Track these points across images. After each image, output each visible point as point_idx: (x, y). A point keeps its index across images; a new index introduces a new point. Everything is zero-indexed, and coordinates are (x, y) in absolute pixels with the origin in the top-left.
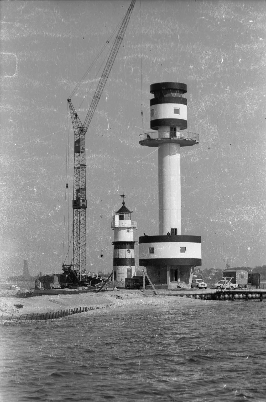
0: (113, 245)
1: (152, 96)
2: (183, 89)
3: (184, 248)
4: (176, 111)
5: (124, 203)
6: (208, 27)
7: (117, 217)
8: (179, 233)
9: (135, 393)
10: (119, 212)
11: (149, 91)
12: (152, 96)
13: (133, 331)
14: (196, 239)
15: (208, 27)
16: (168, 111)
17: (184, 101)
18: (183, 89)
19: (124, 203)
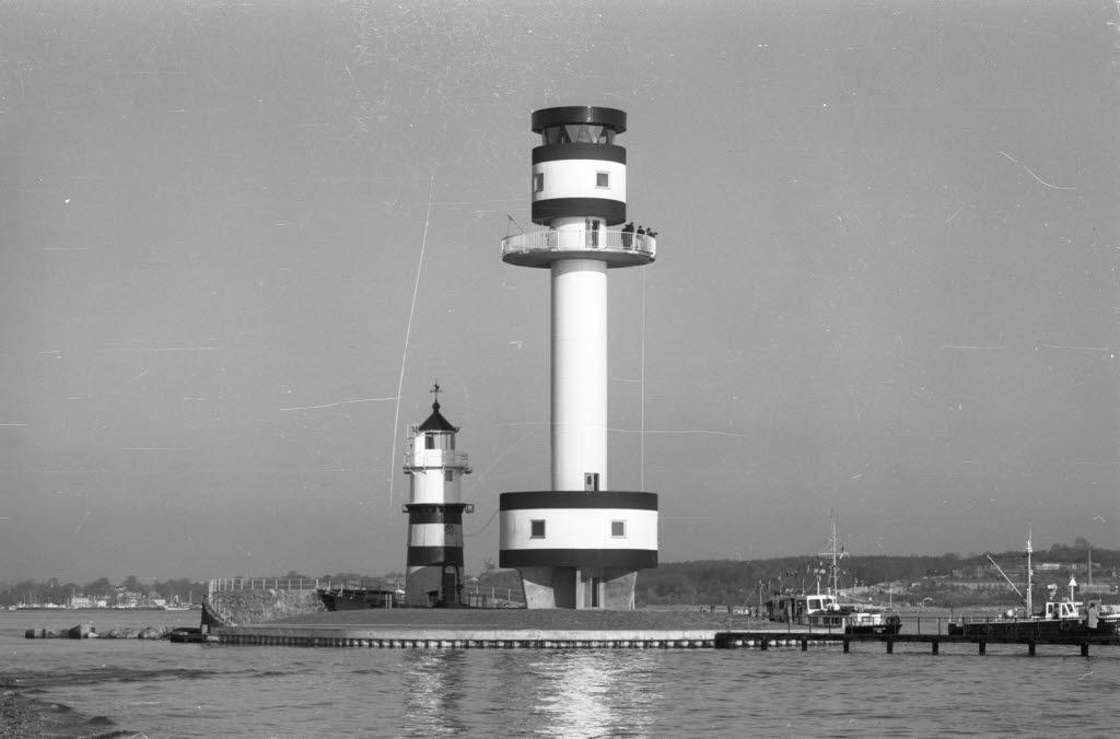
0: (408, 514)
1: (538, 140)
2: (612, 120)
3: (430, 510)
4: (602, 179)
5: (436, 406)
6: (1050, 587)
7: (421, 440)
8: (603, 487)
9: (1003, 578)
10: (422, 428)
11: (530, 128)
12: (538, 140)
13: (964, 580)
14: (645, 501)
15: (1050, 587)
16: (571, 178)
17: (619, 155)
18: (612, 120)
19: (436, 406)
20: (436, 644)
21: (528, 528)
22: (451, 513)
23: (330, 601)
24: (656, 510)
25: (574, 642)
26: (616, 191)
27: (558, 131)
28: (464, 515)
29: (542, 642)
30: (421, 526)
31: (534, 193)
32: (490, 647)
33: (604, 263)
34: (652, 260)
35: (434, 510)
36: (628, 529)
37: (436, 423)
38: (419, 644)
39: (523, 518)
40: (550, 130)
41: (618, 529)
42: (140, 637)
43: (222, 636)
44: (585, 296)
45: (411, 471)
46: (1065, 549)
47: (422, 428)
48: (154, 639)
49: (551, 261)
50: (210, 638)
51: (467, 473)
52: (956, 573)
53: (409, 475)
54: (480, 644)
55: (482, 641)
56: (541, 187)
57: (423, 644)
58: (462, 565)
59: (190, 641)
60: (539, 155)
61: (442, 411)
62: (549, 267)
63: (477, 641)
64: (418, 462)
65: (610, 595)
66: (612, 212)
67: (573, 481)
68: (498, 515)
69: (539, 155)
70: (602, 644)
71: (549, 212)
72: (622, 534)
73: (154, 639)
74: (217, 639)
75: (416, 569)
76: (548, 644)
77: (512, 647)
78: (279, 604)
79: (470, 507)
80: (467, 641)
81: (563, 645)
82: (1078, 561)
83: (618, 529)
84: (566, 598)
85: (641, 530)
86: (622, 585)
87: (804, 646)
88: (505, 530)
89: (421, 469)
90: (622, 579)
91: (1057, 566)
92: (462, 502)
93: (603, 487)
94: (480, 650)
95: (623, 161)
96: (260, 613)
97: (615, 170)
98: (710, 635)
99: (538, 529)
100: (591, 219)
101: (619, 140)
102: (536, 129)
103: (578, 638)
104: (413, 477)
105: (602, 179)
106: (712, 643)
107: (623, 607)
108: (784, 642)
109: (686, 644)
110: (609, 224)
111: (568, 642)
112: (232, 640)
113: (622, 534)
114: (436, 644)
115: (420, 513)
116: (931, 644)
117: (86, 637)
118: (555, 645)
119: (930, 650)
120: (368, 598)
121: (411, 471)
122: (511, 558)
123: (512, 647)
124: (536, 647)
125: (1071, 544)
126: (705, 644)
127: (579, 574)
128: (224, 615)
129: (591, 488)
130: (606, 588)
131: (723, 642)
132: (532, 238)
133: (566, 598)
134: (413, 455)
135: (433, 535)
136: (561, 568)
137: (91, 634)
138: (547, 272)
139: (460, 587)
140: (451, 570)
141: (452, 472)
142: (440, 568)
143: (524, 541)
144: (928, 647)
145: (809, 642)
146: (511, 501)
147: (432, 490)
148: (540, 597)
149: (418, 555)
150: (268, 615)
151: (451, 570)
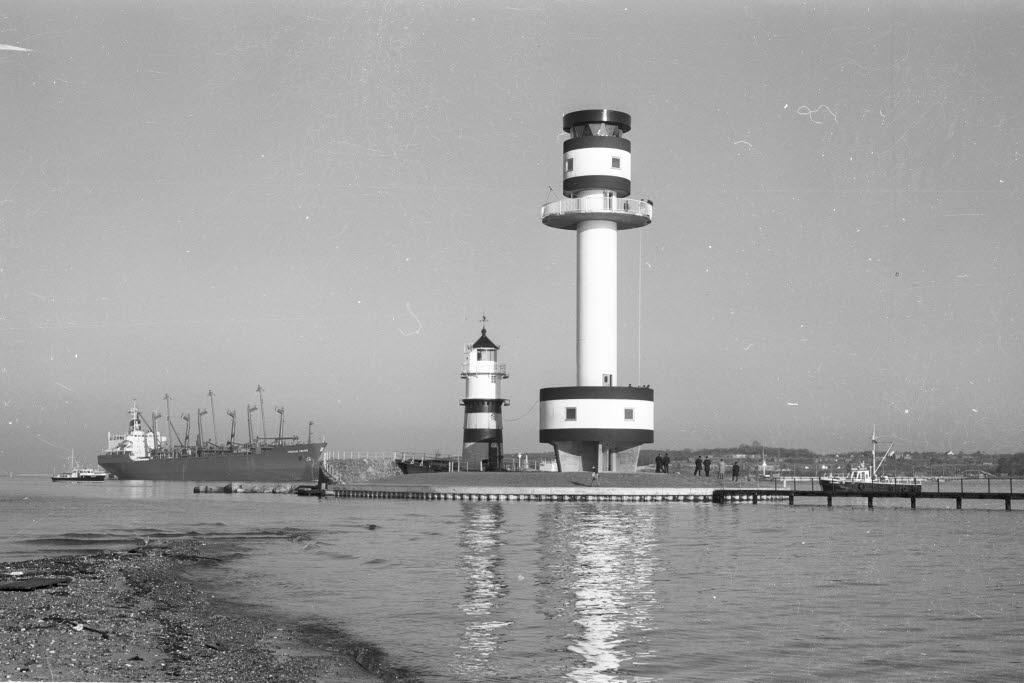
1: (568, 136)
2: (621, 122)
4: (616, 162)
5: (484, 331)
7: (474, 353)
10: (475, 346)
12: (568, 136)
14: (645, 394)
16: (592, 161)
18: (621, 122)
19: (484, 331)
20: (505, 497)
21: (564, 414)
22: (496, 406)
23: (404, 467)
24: (651, 399)
25: (610, 496)
26: (624, 172)
27: (580, 127)
28: (503, 406)
29: (586, 496)
30: (473, 415)
31: (565, 173)
32: (546, 500)
33: (614, 225)
34: (649, 222)
35: (483, 404)
36: (635, 414)
37: (483, 342)
38: (492, 497)
39: (559, 407)
40: (577, 128)
41: (629, 414)
42: (274, 492)
43: (336, 491)
44: (601, 242)
45: (466, 376)
46: (747, 447)
47: (475, 346)
48: (284, 493)
49: (573, 222)
50: (327, 492)
51: (505, 378)
52: (690, 459)
53: (464, 380)
54: (642, 499)
55: (540, 496)
56: (571, 168)
57: (495, 497)
58: (502, 442)
59: (313, 495)
60: (569, 146)
61: (488, 335)
62: (575, 229)
63: (536, 496)
64: (472, 370)
65: (621, 463)
66: (621, 187)
67: (593, 379)
68: (538, 404)
69: (569, 146)
70: (631, 498)
71: (575, 186)
72: (541, 441)
73: (284, 493)
74: (332, 493)
75: (469, 445)
76: (543, 498)
77: (563, 500)
78: (370, 469)
79: (507, 402)
80: (529, 495)
81: (602, 498)
82: (755, 453)
83: (629, 414)
84: (590, 463)
85: (644, 415)
86: (630, 455)
87: (755, 501)
88: (544, 415)
89: (474, 374)
90: (629, 451)
91: (744, 456)
92: (502, 398)
93: (614, 384)
94: (539, 503)
95: (628, 150)
96: (358, 475)
97: (624, 156)
98: (709, 492)
99: (571, 414)
100: (609, 191)
101: (625, 136)
102: (567, 129)
103: (613, 493)
104: (468, 380)
105: (616, 162)
106: (710, 498)
107: (630, 471)
108: (737, 497)
109: (692, 498)
110: (619, 196)
111: (605, 496)
112: (344, 494)
113: (541, 441)
114: (505, 497)
115: (473, 406)
116: (955, 500)
117: (236, 491)
118: (596, 498)
119: (1004, 507)
120: (437, 466)
121: (466, 376)
122: (548, 436)
123: (586, 500)
124: (581, 500)
125: (750, 444)
126: (706, 499)
127: (600, 446)
128: (336, 476)
129: (607, 384)
130: (618, 457)
131: (718, 498)
132: (562, 206)
133: (590, 463)
134: (468, 365)
135: (484, 421)
136: (587, 443)
137: (239, 490)
138: (574, 232)
139: (501, 457)
140: (494, 445)
141: (500, 376)
142: (487, 444)
143: (559, 422)
144: (1001, 504)
145: (759, 497)
146: (548, 394)
147: (483, 389)
148: (571, 463)
149: (471, 435)
150: (363, 476)
151: (494, 445)
